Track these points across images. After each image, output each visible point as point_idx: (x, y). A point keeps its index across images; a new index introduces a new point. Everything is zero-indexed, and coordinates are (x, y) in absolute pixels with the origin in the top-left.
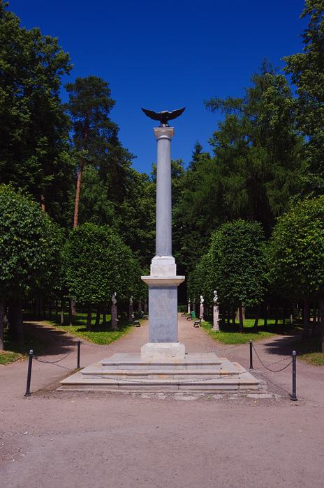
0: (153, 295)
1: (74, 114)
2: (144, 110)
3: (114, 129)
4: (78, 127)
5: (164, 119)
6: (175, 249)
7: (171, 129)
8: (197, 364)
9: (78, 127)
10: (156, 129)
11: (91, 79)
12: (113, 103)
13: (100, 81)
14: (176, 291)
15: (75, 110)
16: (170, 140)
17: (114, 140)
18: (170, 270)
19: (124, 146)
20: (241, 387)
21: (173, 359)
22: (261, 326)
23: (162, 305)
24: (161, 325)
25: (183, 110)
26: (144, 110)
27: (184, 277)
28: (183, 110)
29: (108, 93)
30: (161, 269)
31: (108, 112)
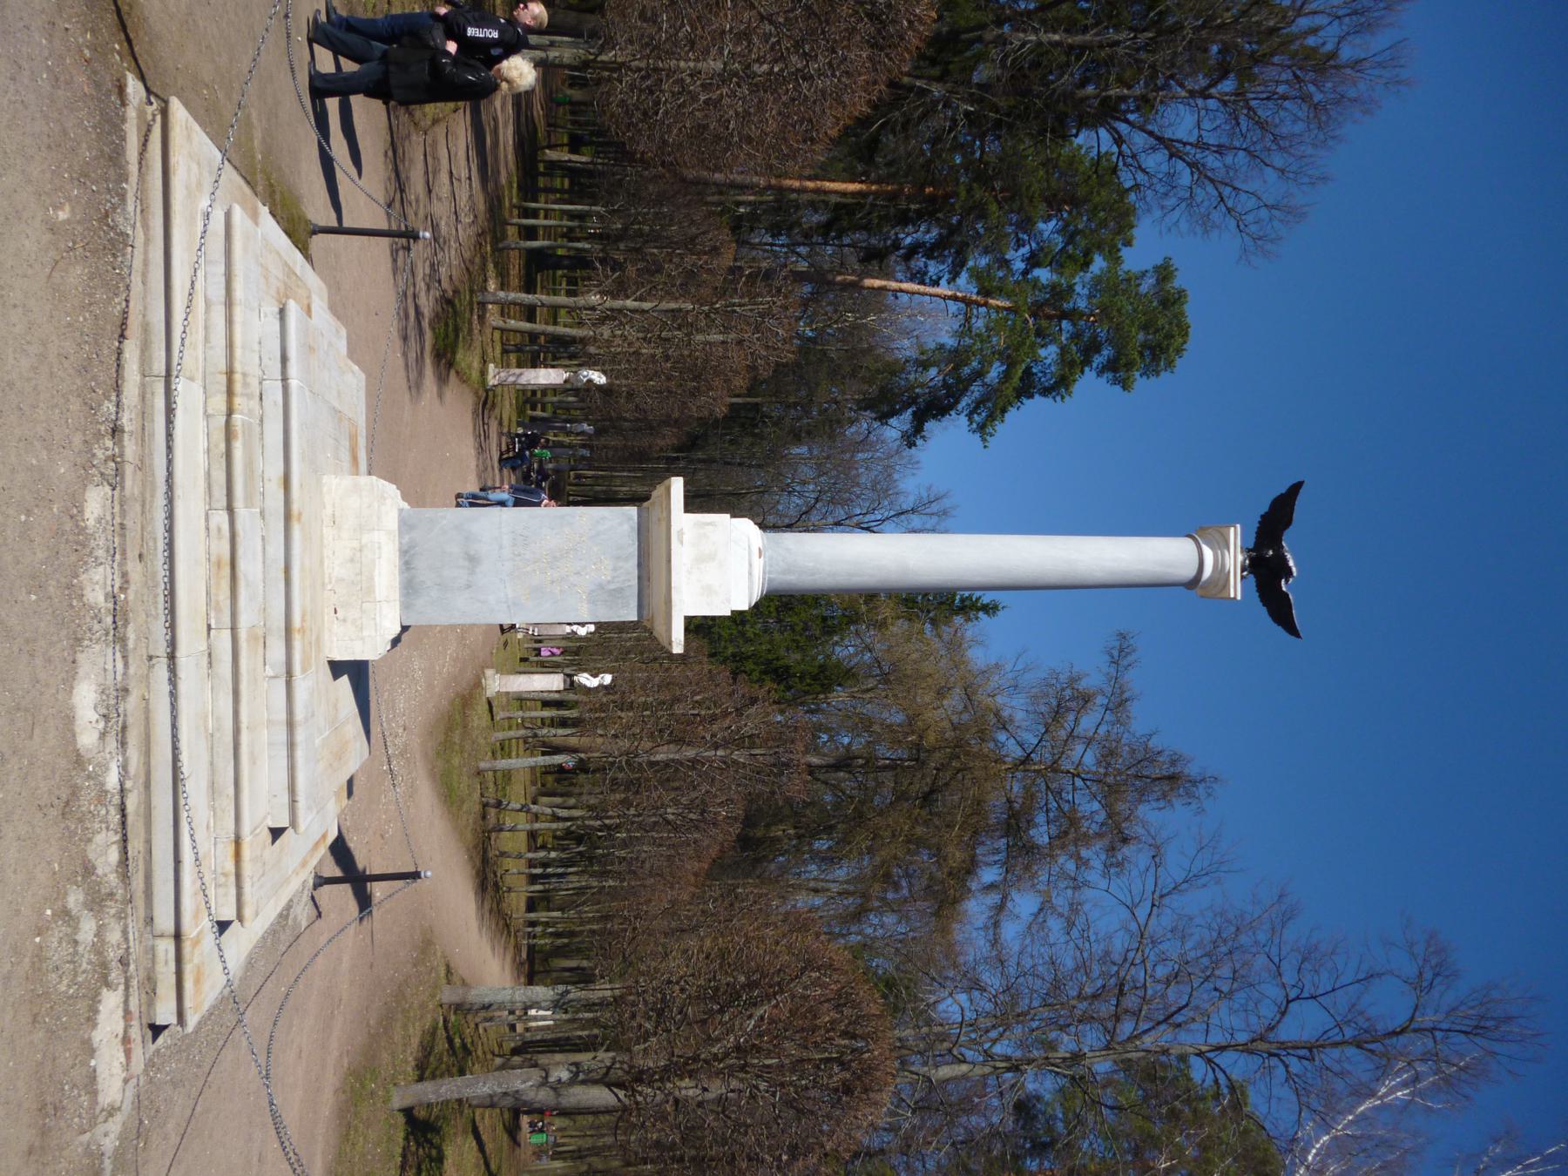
0: (613, 524)
1: (1097, 281)
2: (1296, 488)
3: (1060, 386)
4: (1059, 293)
5: (1266, 568)
6: (782, 606)
7: (1235, 589)
8: (290, 725)
9: (1059, 293)
10: (1235, 535)
11: (1184, 331)
12: (1125, 385)
13: (1179, 351)
14: (635, 618)
15: (1111, 287)
16: (1194, 583)
17: (1026, 389)
18: (708, 590)
19: (1012, 414)
20: (166, 947)
21: (112, 1136)
22: (332, 95)
23: (561, 564)
24: (473, 560)
25: (1292, 629)
26: (1296, 488)
27: (678, 648)
28: (1292, 629)
29: (1152, 370)
30: (711, 557)
31: (1100, 373)
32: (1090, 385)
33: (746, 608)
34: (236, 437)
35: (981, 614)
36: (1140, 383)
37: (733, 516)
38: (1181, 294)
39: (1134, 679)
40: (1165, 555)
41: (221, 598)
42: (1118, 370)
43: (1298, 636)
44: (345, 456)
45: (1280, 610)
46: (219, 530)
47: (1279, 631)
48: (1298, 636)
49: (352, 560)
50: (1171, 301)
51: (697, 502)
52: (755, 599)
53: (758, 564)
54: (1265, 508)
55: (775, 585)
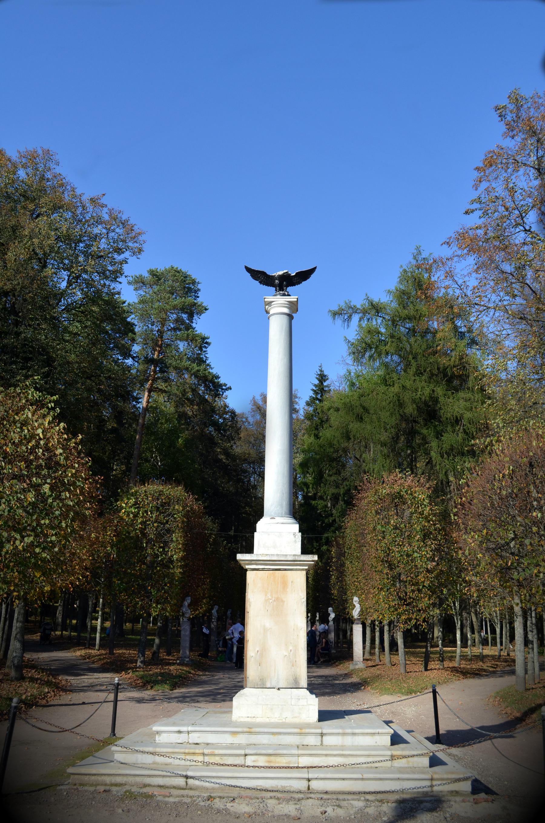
2: (248, 270)
5: (284, 283)
25: (312, 271)
26: (248, 270)
27: (316, 558)
28: (312, 271)
32: (201, 325)
33: (298, 525)
34: (213, 752)
35: (325, 384)
36: (203, 299)
37: (256, 531)
38: (153, 273)
39: (359, 302)
40: (277, 328)
41: (284, 761)
42: (193, 310)
43: (315, 268)
44: (225, 715)
45: (304, 276)
46: (254, 761)
47: (316, 270)
48: (315, 268)
49: (272, 709)
50: (157, 277)
51: (250, 549)
52: (294, 521)
53: (279, 519)
54: (257, 282)
55: (287, 511)
